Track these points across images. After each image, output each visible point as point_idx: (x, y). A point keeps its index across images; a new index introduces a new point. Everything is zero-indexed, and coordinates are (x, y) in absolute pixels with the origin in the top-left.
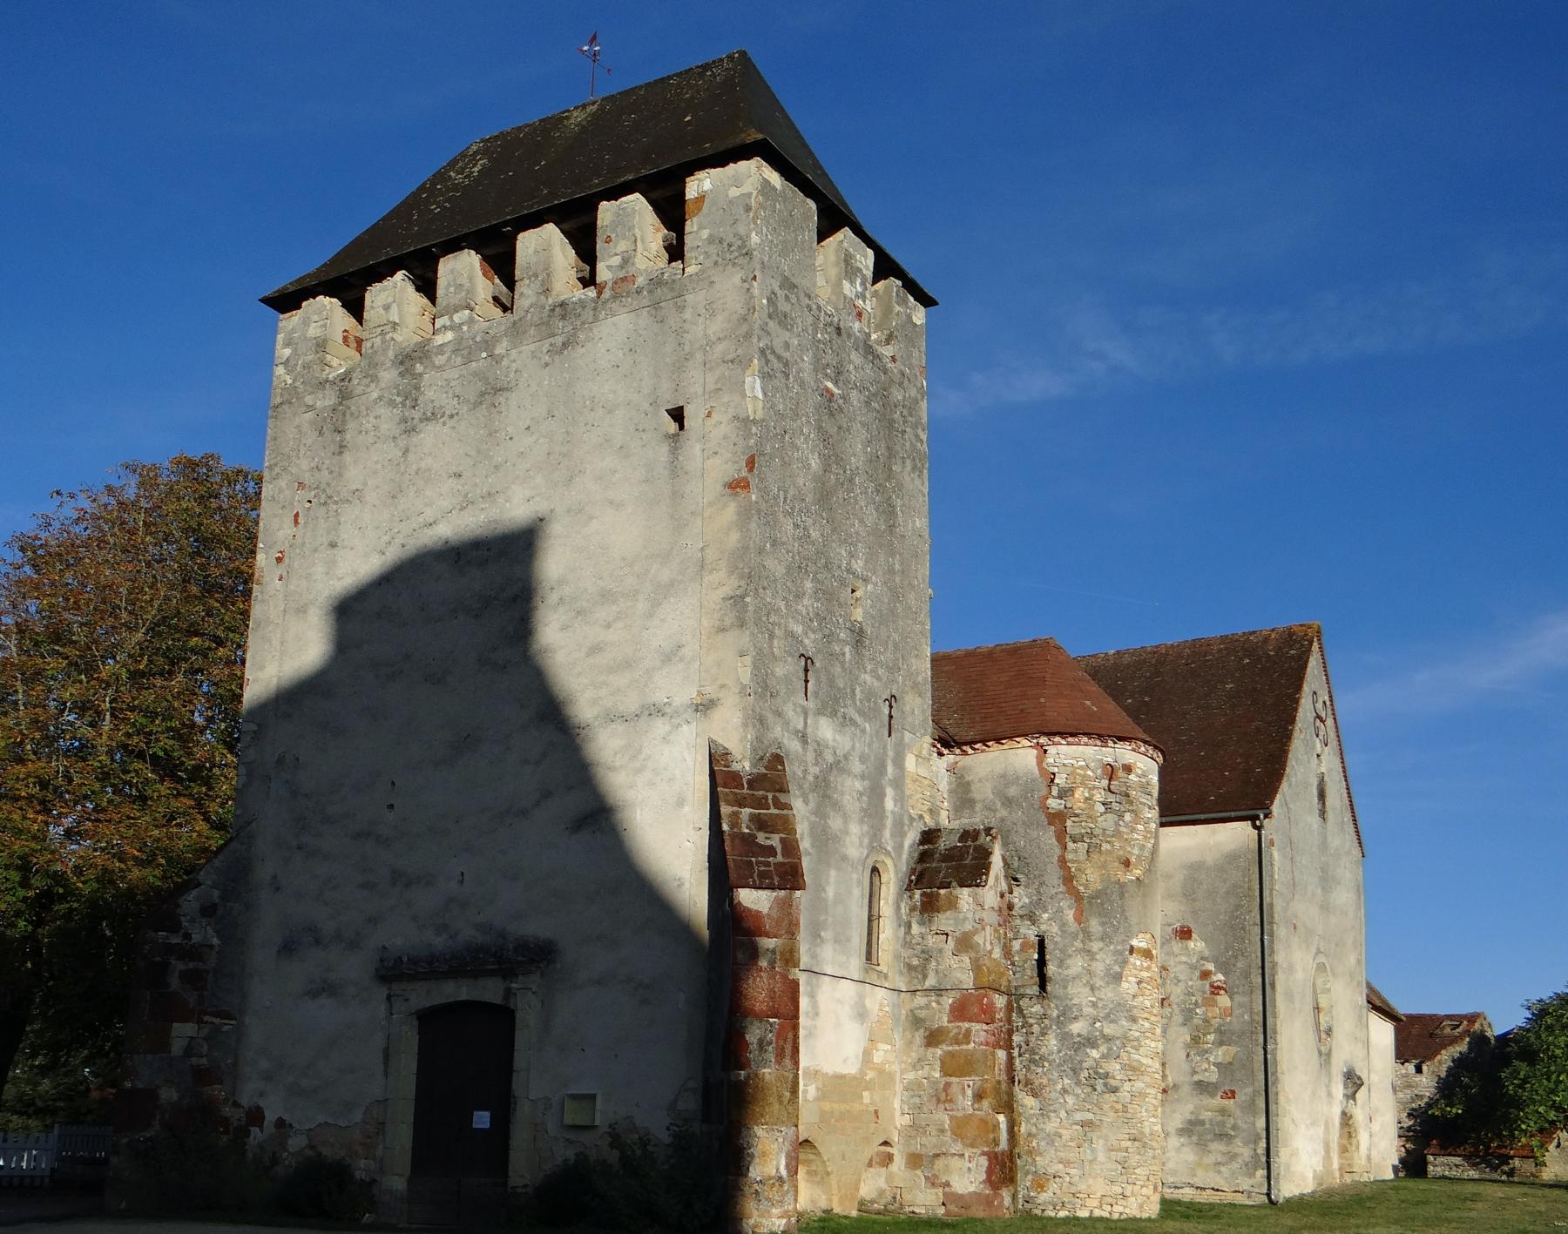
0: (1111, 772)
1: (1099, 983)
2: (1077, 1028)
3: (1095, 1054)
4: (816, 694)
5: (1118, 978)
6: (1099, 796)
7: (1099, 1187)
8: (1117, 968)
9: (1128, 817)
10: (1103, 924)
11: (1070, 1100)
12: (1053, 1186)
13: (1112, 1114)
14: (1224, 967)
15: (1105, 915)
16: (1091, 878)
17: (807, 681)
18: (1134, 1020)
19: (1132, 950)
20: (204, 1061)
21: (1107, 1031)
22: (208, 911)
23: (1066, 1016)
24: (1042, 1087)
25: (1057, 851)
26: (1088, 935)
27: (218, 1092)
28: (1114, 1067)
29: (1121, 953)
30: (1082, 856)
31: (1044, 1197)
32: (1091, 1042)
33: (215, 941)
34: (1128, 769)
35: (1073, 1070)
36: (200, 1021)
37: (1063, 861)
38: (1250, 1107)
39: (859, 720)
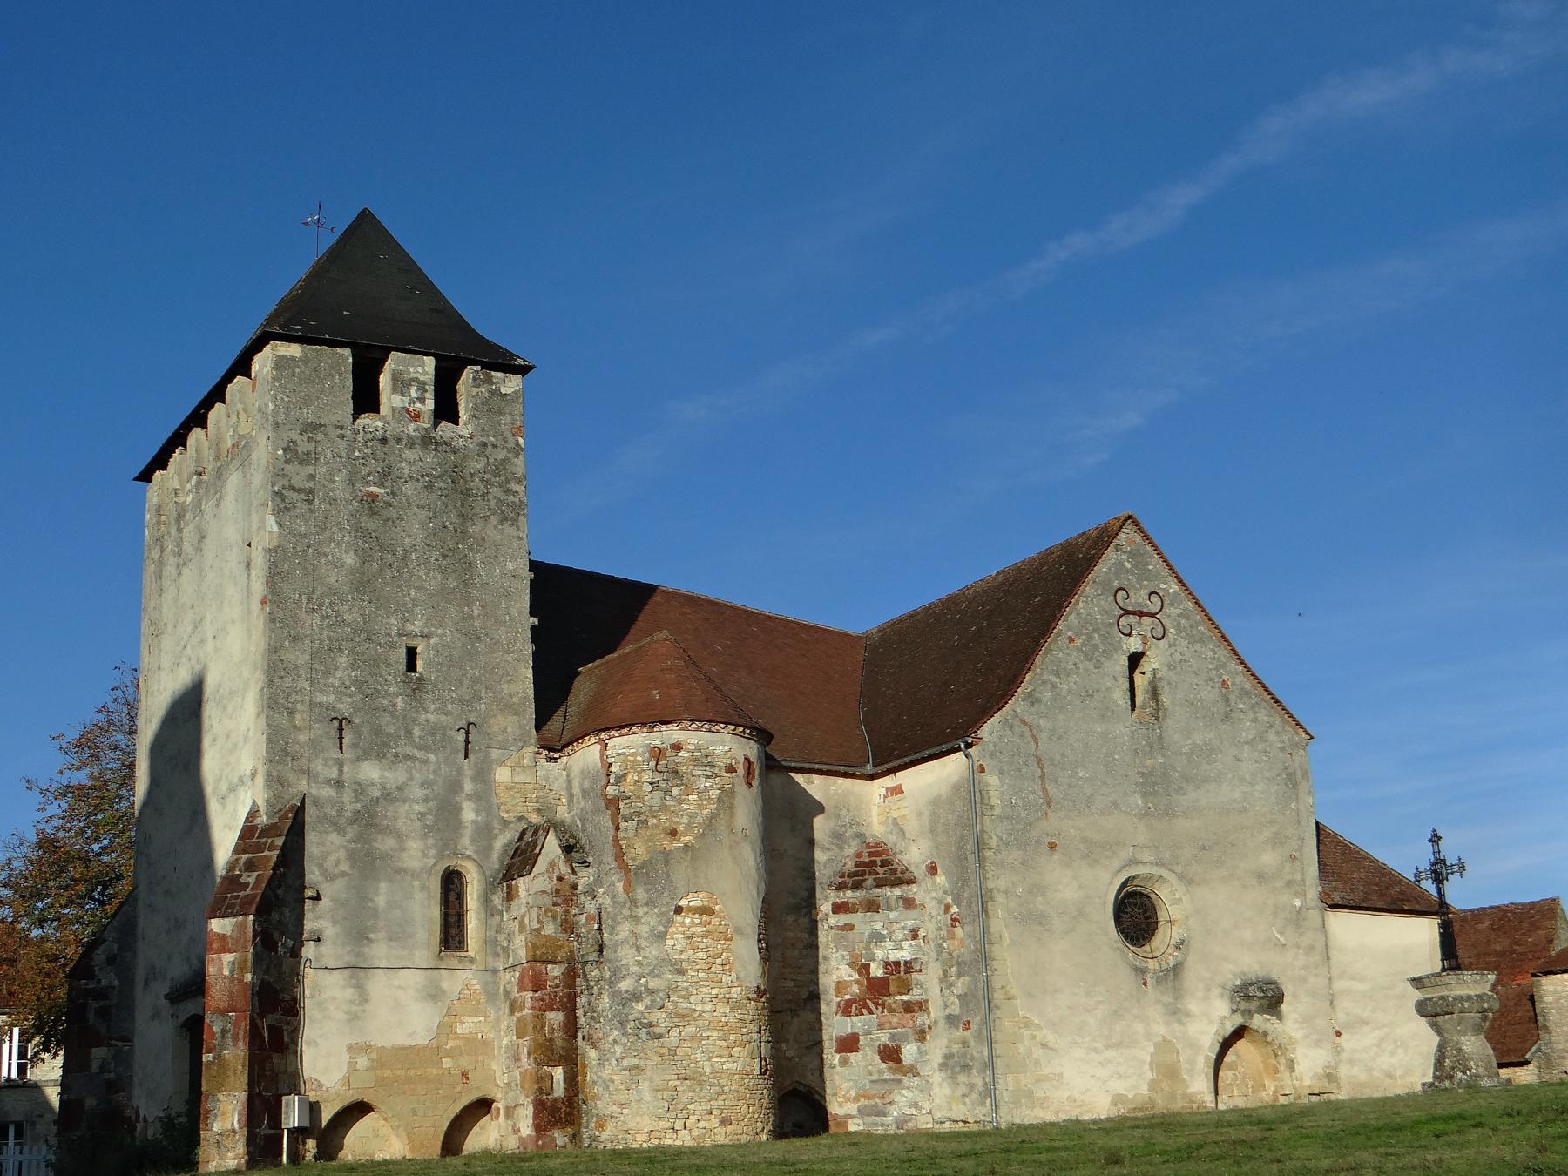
0: (657, 754)
1: (644, 944)
2: (625, 985)
3: (640, 1006)
4: (355, 746)
5: (662, 937)
6: (646, 778)
7: (647, 1124)
8: (661, 928)
9: (675, 791)
10: (648, 891)
11: (618, 1049)
12: (610, 1126)
13: (657, 1058)
14: (958, 902)
15: (650, 883)
16: (639, 851)
17: (341, 738)
18: (681, 972)
19: (679, 910)
20: (112, 1075)
21: (651, 985)
22: (111, 960)
23: (617, 976)
24: (599, 1039)
25: (612, 832)
26: (634, 903)
27: (120, 1097)
28: (659, 1017)
29: (664, 914)
30: (631, 833)
31: (604, 1136)
32: (636, 997)
33: (116, 983)
34: (677, 747)
35: (621, 1023)
36: (109, 1045)
37: (616, 840)
38: (978, 1037)
39: (417, 753)
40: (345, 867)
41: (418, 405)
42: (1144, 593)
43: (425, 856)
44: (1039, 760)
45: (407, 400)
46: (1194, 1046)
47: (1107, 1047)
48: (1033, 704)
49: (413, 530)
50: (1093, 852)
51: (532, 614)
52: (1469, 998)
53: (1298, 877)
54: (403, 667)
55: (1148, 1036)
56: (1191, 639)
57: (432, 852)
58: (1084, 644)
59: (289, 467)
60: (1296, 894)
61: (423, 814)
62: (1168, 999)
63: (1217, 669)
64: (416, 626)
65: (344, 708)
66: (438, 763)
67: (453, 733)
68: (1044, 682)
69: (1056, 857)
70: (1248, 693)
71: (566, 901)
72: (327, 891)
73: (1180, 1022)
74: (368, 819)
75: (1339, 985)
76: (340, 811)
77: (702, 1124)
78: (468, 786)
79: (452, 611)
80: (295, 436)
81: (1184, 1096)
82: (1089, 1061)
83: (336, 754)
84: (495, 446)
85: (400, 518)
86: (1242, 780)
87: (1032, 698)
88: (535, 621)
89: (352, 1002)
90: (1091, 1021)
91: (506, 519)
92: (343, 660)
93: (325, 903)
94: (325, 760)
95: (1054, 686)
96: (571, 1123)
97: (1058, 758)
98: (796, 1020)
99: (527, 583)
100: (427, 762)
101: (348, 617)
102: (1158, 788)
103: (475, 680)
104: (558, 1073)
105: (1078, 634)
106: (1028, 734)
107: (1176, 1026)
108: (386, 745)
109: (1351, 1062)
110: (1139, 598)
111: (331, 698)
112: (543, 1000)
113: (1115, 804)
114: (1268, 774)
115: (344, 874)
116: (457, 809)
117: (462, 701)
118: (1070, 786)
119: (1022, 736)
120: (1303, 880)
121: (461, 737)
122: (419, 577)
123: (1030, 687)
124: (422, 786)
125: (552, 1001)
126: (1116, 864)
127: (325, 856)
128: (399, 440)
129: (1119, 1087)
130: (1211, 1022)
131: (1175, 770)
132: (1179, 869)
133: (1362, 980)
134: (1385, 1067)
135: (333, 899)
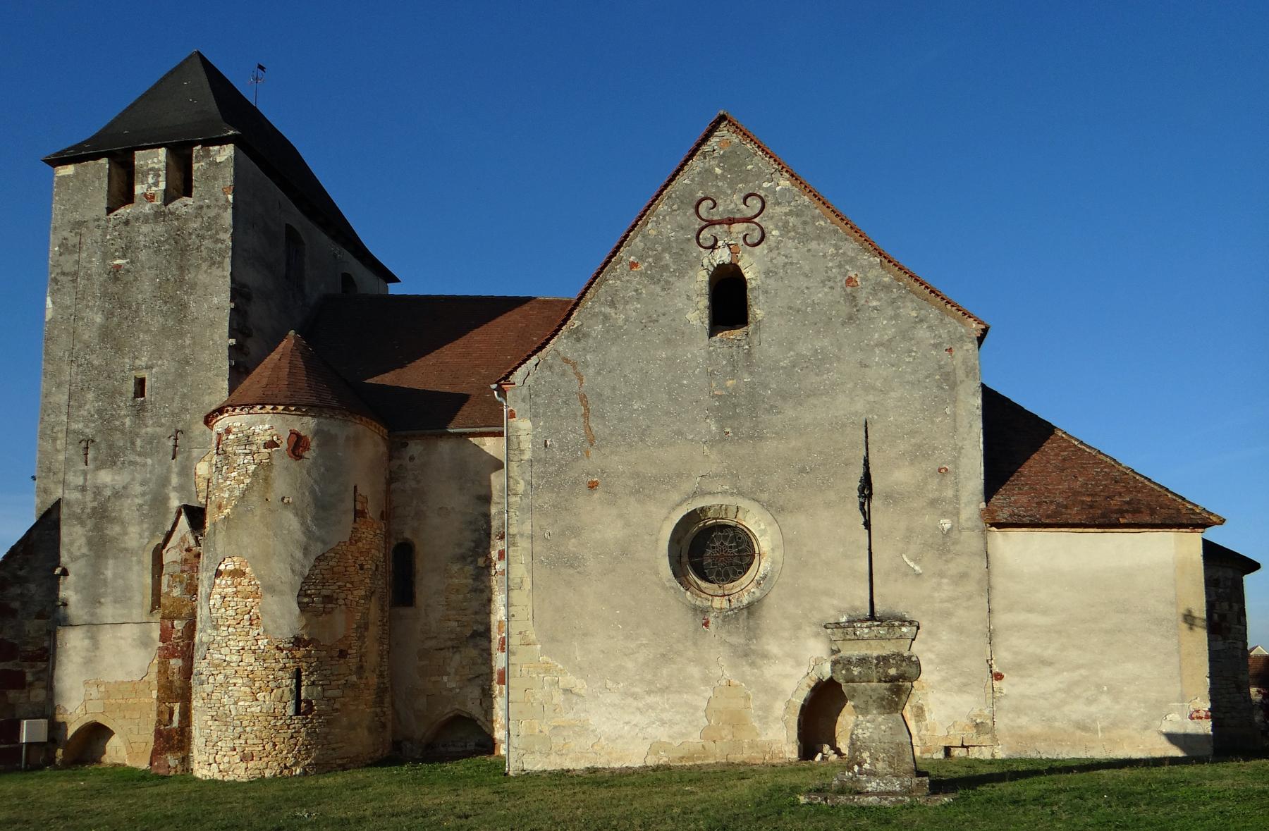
4: (95, 459)
39: (138, 459)
40: (85, 550)
41: (154, 188)
42: (737, 198)
43: (141, 537)
44: (583, 398)
45: (145, 186)
46: (772, 691)
47: (649, 693)
48: (578, 340)
49: (144, 289)
50: (643, 487)
51: (231, 336)
52: (863, 661)
53: (949, 493)
54: (131, 395)
55: (706, 680)
56: (804, 238)
57: (146, 534)
58: (650, 267)
59: (62, 258)
60: (944, 515)
61: (141, 506)
62: (737, 640)
63: (840, 266)
64: (141, 362)
65: (89, 432)
66: (153, 465)
67: (165, 440)
68: (595, 315)
69: (596, 496)
70: (887, 288)
71: (192, 568)
72: (72, 568)
73: (753, 664)
74: (102, 515)
75: (1001, 619)
76: (83, 510)
77: (226, 759)
78: (175, 480)
79: (169, 345)
80: (66, 234)
81: (752, 745)
82: (702, 700)
83: (82, 467)
84: (208, 207)
85: (136, 280)
86: (868, 388)
87: (578, 335)
88: (233, 341)
89: (88, 650)
90: (630, 665)
91: (214, 263)
92: (90, 396)
93: (71, 578)
94: (75, 472)
95: (606, 317)
96: (181, 749)
97: (607, 392)
98: (457, 657)
99: (227, 311)
100: (145, 465)
101: (96, 363)
102: (737, 415)
103: (184, 396)
104: (177, 707)
105: (642, 258)
106: (571, 372)
107: (747, 669)
108: (117, 455)
109: (1017, 710)
110: (731, 203)
111: (81, 426)
112: (167, 649)
113: (679, 433)
114: (909, 378)
115: (84, 555)
116: (166, 499)
117: (173, 414)
118: (621, 420)
119: (564, 374)
120: (956, 496)
121: (171, 443)
122: (147, 323)
123: (577, 323)
124: (141, 484)
125: (175, 650)
126: (676, 497)
127: (72, 543)
128: (137, 219)
129: (662, 734)
130: (799, 664)
131: (766, 387)
132: (765, 497)
133: (1045, 612)
134: (1074, 717)
135: (77, 575)
